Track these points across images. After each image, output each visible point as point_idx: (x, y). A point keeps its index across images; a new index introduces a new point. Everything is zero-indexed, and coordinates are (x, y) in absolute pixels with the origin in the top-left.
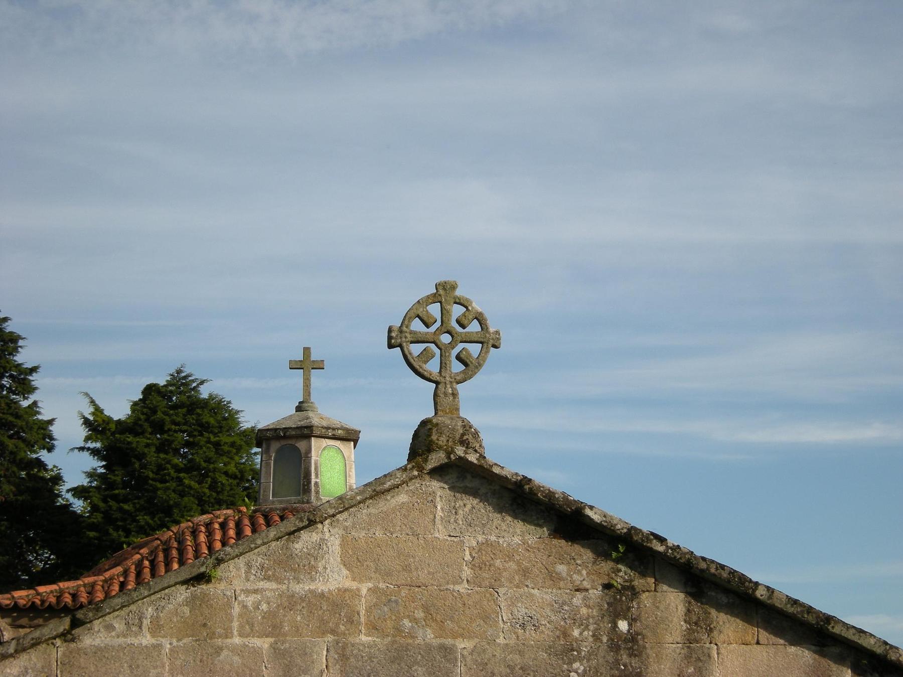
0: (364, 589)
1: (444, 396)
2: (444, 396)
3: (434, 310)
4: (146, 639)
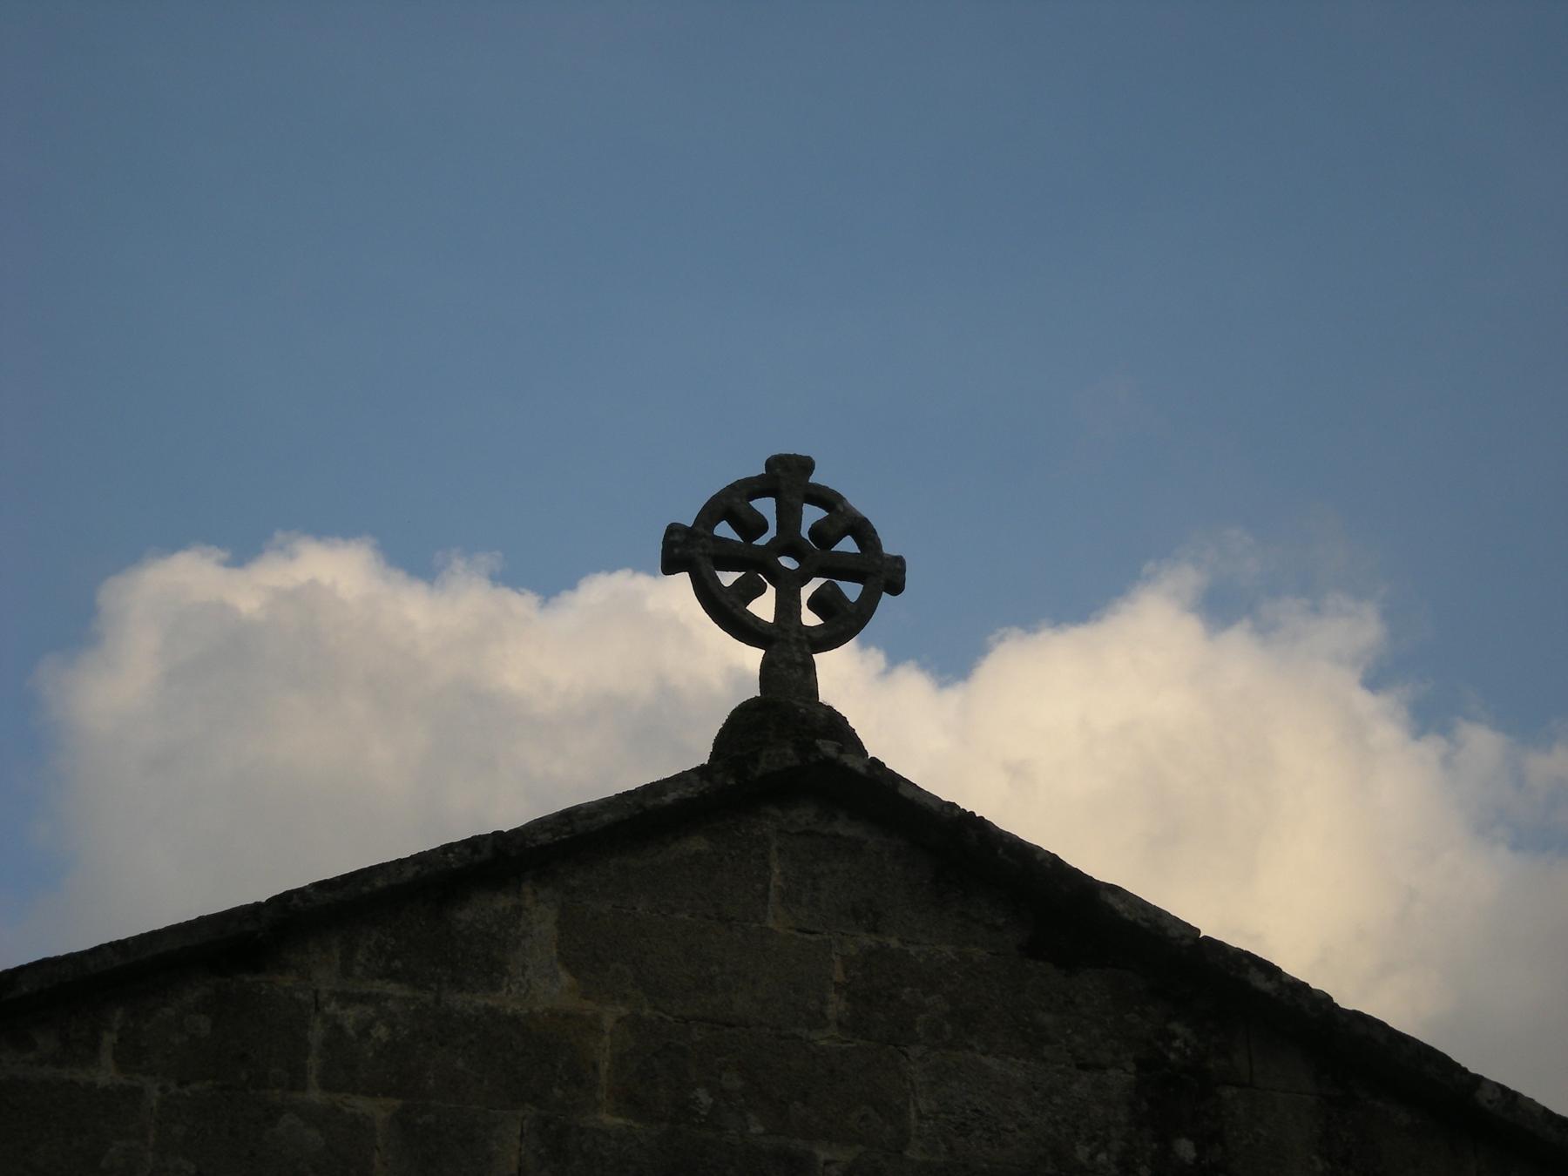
0: (611, 1015)
1: (788, 655)
2: (788, 655)
3: (766, 507)
4: (105, 1074)
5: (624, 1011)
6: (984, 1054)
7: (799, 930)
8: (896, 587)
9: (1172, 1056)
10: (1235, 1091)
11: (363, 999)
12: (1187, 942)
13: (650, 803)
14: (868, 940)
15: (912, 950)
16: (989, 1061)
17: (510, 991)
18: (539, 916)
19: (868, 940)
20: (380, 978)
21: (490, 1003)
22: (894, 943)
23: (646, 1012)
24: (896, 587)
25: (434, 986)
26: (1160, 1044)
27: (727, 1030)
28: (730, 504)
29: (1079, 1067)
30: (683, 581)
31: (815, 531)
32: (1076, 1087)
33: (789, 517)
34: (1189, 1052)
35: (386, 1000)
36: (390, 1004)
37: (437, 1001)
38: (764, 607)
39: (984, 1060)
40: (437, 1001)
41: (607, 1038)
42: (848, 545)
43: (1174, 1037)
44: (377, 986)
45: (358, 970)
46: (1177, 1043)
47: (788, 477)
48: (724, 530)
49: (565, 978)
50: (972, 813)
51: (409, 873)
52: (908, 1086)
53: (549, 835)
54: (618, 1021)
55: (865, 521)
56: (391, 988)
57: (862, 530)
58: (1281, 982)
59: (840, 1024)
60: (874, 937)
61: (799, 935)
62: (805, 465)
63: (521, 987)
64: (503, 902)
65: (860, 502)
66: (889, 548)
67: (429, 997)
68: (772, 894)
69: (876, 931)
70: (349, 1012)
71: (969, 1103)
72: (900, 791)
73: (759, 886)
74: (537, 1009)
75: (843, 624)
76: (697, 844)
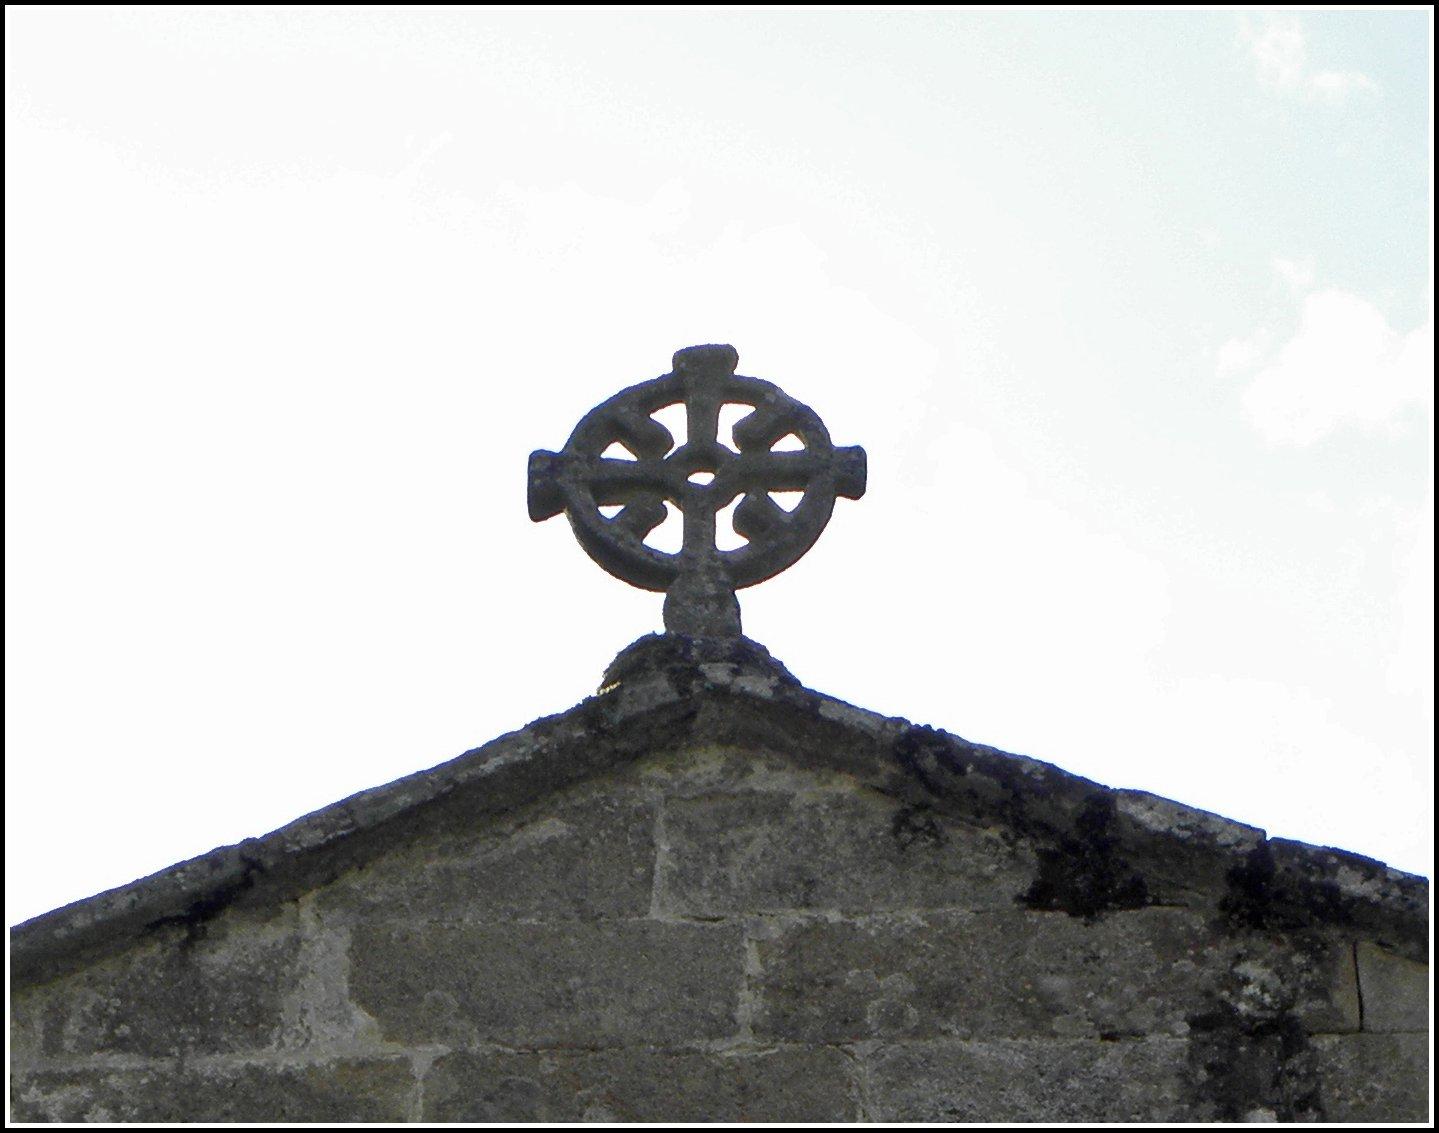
2: (702, 590)
3: (674, 419)
5: (443, 1049)
6: (966, 1039)
7: (697, 919)
8: (855, 488)
9: (1243, 1007)
10: (1336, 1039)
11: (74, 1079)
12: (1247, 848)
13: (462, 777)
14: (797, 917)
15: (860, 922)
16: (973, 1047)
17: (282, 1044)
18: (321, 937)
19: (797, 917)
20: (101, 1049)
21: (253, 1062)
22: (834, 916)
23: (476, 1047)
24: (855, 488)
25: (175, 1050)
26: (1225, 994)
27: (591, 1055)
28: (624, 415)
29: (1105, 1037)
30: (560, 525)
31: (741, 432)
32: (1100, 1063)
33: (703, 423)
34: (1267, 999)
35: (106, 1076)
36: (113, 1080)
37: (179, 1069)
38: (667, 537)
39: (965, 1046)
40: (179, 1069)
41: (419, 1084)
42: (790, 444)
43: (1246, 981)
44: (95, 1061)
45: (68, 1044)
46: (1250, 990)
47: (704, 373)
48: (617, 451)
49: (361, 1018)
50: (928, 727)
51: (122, 904)
52: (855, 1092)
53: (319, 833)
54: (436, 1063)
55: (808, 409)
56: (118, 1061)
57: (802, 419)
58: (1387, 880)
59: (755, 1028)
60: (804, 912)
61: (696, 924)
62: (724, 356)
63: (298, 1035)
64: (273, 935)
65: (797, 388)
66: (841, 437)
67: (167, 1065)
68: (657, 879)
69: (808, 905)
70: (55, 1096)
71: (943, 1103)
72: (821, 711)
73: (639, 870)
74: (320, 1061)
75: (778, 546)
76: (551, 828)
